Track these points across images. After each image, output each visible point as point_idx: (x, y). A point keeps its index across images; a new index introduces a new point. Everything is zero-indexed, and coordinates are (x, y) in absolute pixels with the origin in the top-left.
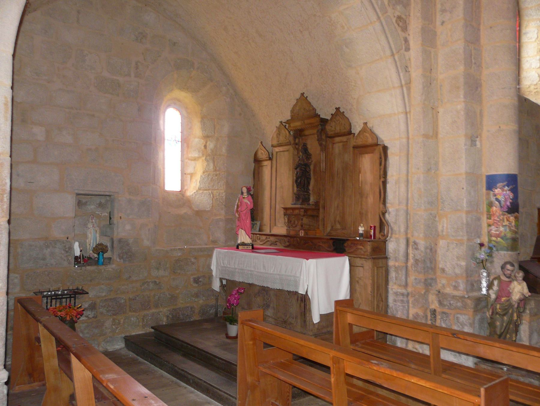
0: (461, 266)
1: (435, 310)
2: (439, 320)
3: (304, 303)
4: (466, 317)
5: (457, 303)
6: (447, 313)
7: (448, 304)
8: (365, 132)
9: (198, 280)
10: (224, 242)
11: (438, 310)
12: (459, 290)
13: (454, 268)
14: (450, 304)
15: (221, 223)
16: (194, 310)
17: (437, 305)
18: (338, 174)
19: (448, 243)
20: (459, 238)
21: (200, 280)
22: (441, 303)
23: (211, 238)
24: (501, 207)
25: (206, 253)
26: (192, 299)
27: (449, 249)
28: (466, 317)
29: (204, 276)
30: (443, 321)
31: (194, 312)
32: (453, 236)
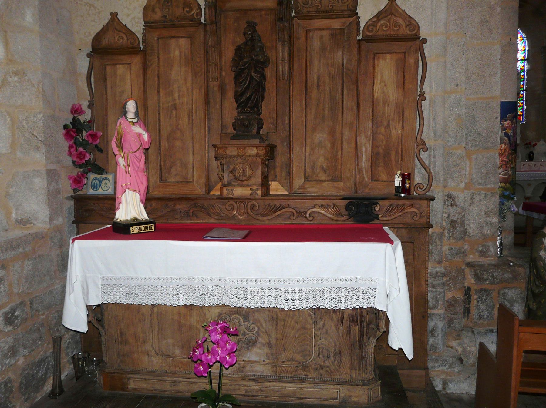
0: (491, 224)
1: (469, 289)
2: (475, 301)
3: (361, 325)
4: (518, 291)
5: (503, 274)
6: (488, 290)
7: (490, 278)
8: (392, 14)
9: (13, 314)
10: (48, 220)
11: (474, 287)
12: (489, 256)
13: (482, 227)
14: (493, 277)
15: (37, 181)
16: (10, 387)
17: (473, 281)
18: (318, 86)
19: (473, 194)
20: (489, 186)
21: (16, 314)
22: (478, 278)
23: (14, 215)
24: (510, 144)
25: (21, 250)
26: (5, 364)
27: (473, 202)
28: (518, 291)
29: (22, 304)
30: (481, 301)
31: (11, 392)
32: (480, 184)
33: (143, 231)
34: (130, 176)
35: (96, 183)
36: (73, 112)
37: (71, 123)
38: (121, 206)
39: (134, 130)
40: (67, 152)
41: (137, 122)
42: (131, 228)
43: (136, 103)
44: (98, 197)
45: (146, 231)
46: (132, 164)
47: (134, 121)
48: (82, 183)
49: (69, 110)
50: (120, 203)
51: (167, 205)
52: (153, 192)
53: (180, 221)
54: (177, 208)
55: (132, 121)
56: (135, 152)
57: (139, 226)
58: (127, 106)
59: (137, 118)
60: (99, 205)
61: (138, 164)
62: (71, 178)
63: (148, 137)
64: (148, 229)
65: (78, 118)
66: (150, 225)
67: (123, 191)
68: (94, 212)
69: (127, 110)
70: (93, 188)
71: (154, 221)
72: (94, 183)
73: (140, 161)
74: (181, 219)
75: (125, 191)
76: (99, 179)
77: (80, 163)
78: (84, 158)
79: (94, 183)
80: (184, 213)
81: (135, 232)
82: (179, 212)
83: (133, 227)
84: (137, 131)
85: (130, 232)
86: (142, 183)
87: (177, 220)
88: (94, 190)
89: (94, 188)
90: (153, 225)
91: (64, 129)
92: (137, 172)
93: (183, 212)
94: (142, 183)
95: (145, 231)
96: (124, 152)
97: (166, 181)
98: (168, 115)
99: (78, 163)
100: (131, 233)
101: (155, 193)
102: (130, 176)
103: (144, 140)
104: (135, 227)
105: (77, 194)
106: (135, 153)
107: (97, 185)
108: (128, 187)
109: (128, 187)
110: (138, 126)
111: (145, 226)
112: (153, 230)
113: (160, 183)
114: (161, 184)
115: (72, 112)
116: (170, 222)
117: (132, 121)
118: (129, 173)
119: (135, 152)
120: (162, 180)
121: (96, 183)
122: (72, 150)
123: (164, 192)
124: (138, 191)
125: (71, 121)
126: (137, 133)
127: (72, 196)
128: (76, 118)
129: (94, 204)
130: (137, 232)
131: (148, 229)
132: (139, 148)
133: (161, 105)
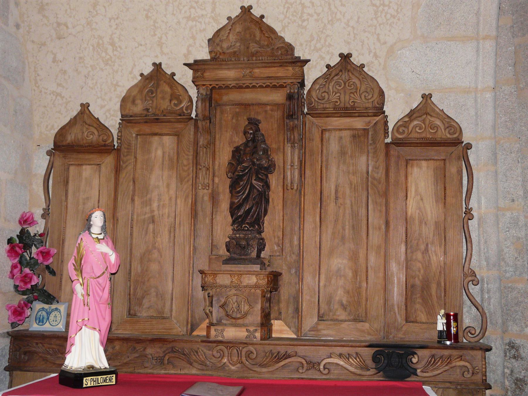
33: (101, 384)
35: (43, 316)
36: (22, 222)
37: (17, 236)
38: (73, 348)
39: (99, 249)
40: (9, 273)
41: (103, 239)
42: (85, 379)
43: (104, 215)
44: (43, 335)
46: (93, 293)
47: (99, 238)
48: (23, 315)
50: (72, 345)
52: (117, 329)
53: (150, 371)
54: (147, 353)
55: (97, 238)
56: (99, 277)
57: (95, 377)
58: (92, 219)
59: (104, 234)
60: (44, 346)
61: (101, 293)
62: (10, 308)
64: (108, 381)
65: (27, 230)
66: (110, 376)
67: (78, 329)
68: (36, 354)
70: (37, 322)
72: (40, 315)
73: (104, 289)
75: (81, 329)
76: (47, 310)
78: (30, 282)
79: (40, 315)
81: (89, 385)
84: (102, 251)
86: (104, 319)
90: (114, 375)
91: (8, 244)
92: (98, 304)
93: (156, 358)
94: (104, 319)
98: (143, 229)
100: (84, 386)
101: (119, 332)
104: (90, 378)
105: (15, 329)
107: (43, 318)
108: (85, 323)
110: (104, 244)
111: (103, 376)
112: (114, 383)
114: (129, 319)
116: (137, 371)
117: (97, 238)
118: (87, 305)
119: (99, 277)
120: (129, 314)
121: (43, 316)
122: (16, 271)
124: (98, 329)
126: (102, 253)
129: (37, 344)
130: (92, 385)
132: (104, 272)
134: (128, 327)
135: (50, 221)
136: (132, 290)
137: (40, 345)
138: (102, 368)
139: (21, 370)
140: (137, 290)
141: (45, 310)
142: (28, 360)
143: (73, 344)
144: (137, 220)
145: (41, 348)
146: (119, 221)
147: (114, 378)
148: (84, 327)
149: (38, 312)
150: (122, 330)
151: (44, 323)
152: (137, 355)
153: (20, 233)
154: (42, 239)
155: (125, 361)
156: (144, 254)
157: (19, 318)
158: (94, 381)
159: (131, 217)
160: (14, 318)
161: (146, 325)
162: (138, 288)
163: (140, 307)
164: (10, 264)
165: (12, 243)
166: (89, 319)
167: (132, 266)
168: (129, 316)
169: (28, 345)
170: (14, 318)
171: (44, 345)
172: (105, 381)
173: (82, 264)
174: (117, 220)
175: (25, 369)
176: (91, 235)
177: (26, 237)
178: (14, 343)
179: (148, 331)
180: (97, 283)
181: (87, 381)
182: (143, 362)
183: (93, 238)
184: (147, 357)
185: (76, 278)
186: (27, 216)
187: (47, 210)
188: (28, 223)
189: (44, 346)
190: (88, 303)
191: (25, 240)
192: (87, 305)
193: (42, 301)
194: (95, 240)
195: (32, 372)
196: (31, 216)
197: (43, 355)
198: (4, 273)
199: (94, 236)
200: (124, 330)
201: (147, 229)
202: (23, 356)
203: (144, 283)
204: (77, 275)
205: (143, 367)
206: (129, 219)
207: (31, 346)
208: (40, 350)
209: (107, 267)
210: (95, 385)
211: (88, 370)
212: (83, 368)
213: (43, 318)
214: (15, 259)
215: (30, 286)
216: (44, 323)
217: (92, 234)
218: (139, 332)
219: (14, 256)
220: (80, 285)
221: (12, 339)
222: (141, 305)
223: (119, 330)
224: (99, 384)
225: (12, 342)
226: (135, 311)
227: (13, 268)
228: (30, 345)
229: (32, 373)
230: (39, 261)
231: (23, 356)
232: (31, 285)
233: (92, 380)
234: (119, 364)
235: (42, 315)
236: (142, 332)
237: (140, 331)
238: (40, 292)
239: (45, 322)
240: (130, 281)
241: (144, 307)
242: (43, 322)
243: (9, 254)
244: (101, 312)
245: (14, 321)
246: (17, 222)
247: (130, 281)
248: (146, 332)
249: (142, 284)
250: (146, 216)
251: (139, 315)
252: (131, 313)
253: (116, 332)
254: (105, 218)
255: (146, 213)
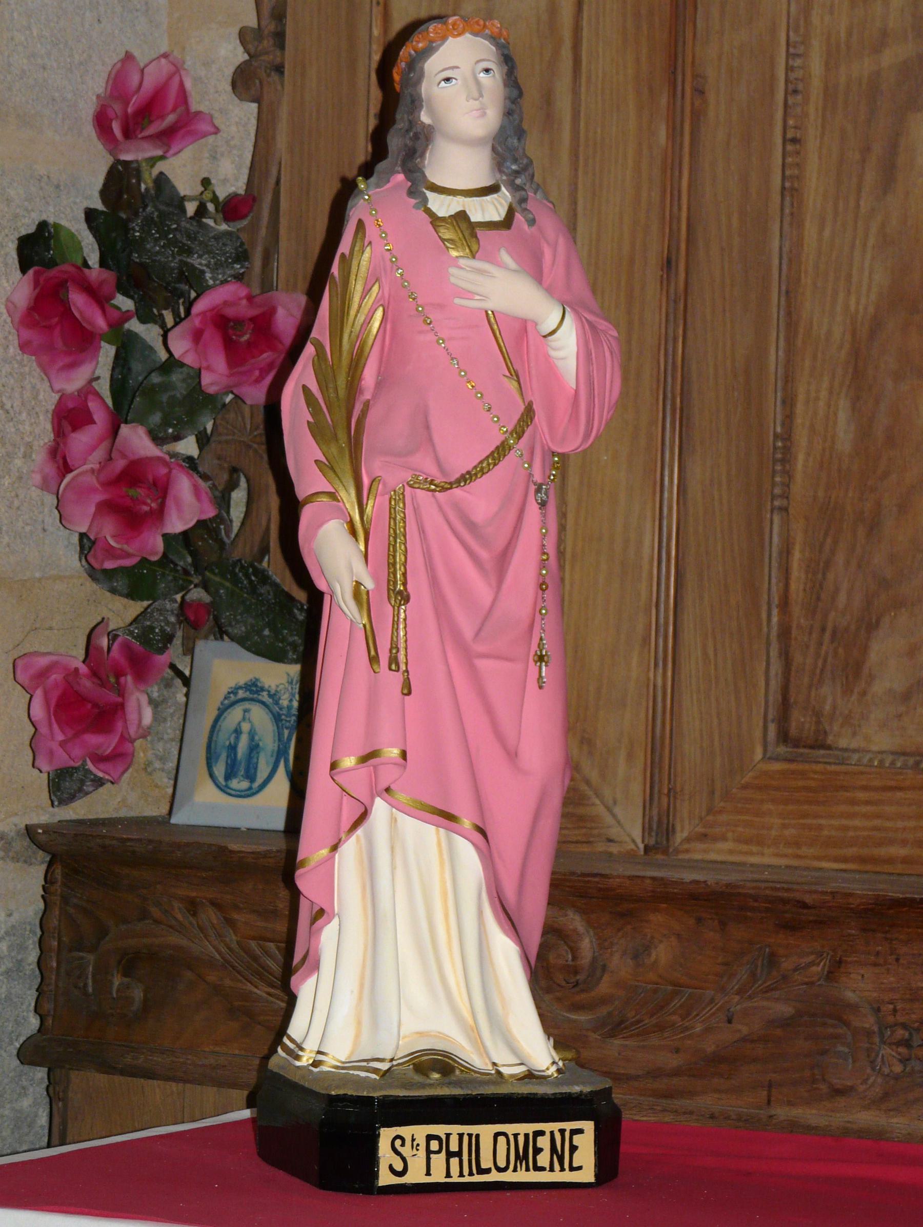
33: (494, 1176)
34: (407, 689)
35: (252, 734)
36: (116, 127)
37: (90, 215)
38: (328, 935)
39: (468, 294)
40: (40, 456)
41: (507, 222)
42: (386, 1135)
43: (508, 60)
44: (223, 850)
45: (558, 1176)
46: (434, 582)
47: (475, 217)
48: (120, 725)
49: (88, 110)
50: (320, 914)
51: (772, 961)
52: (703, 837)
53: (866, 1118)
54: (850, 996)
55: (462, 216)
56: (466, 478)
57: (454, 1129)
58: (425, 89)
59: (515, 188)
60: (230, 923)
61: (483, 590)
62: (42, 675)
63: (586, 356)
64: (544, 1159)
65: (162, 181)
66: (555, 1126)
67: (347, 819)
68: (189, 975)
69: (425, 118)
70: (220, 770)
71: (607, 1092)
72: (238, 732)
73: (503, 558)
74: (885, 1096)
75: (363, 816)
76: (274, 696)
77: (128, 555)
78: (159, 514)
79: (238, 732)
80: (907, 1043)
81: (417, 1175)
82: (869, 1034)
83: (406, 1131)
84: (490, 305)
85: (375, 1175)
86: (512, 755)
87: (841, 1102)
88: (225, 789)
89: (228, 777)
90: (588, 1126)
91: (24, 269)
92: (468, 657)
93: (901, 1033)
94: (512, 755)
95: (509, 1177)
96: (366, 481)
97: (820, 743)
98: (866, 150)
99: (111, 553)
100: (385, 1178)
101: (719, 852)
102: (407, 689)
103: (550, 370)
104: (420, 1131)
105: (78, 810)
106: (457, 492)
107: (254, 748)
108: (387, 776)
109: (387, 776)
110: (505, 257)
111: (510, 1129)
112: (587, 1175)
113: (766, 758)
114: (778, 766)
115: (102, 122)
116: (782, 1113)
117: (462, 216)
118: (393, 660)
119: (466, 478)
120: (784, 737)
121: (252, 734)
122: (81, 440)
123: (797, 845)
124: (467, 824)
125: (99, 205)
126: (491, 319)
127: (30, 831)
128: (138, 173)
129: (193, 906)
130: (438, 1176)
131: (544, 1159)
132: (502, 450)
133: (816, 66)
134: (778, 821)
135: (284, 112)
136: (797, 572)
137: (210, 915)
138: (506, 1071)
139: (108, 1068)
140: (831, 576)
141: (264, 696)
142: (146, 1007)
143: (321, 912)
144: (829, 93)
145: (220, 936)
146: (711, 97)
147: (586, 1143)
148: (380, 807)
149: (222, 711)
150: (738, 840)
151: (259, 781)
152: (785, 1009)
153: (105, 193)
154: (244, 237)
155: (709, 1046)
156: (876, 325)
157: (93, 739)
158: (450, 1155)
159: (789, 69)
160: (62, 744)
161: (889, 809)
162: (840, 558)
163: (848, 690)
164: (49, 400)
165: (51, 264)
166: (404, 755)
167: (800, 408)
168: (782, 749)
169: (144, 915)
170: (62, 744)
171: (236, 916)
172: (522, 1158)
173: (367, 396)
174: (700, 92)
175: (128, 1059)
176: (425, 200)
177: (149, 222)
178: (65, 900)
179: (903, 852)
180: (452, 516)
181: (406, 1151)
182: (824, 1052)
183: (435, 220)
184: (847, 1024)
185: (322, 484)
186: (149, 84)
187: (267, 43)
188: (152, 130)
189: (230, 923)
190: (394, 646)
191: (139, 245)
192: (393, 660)
193: (241, 641)
194: (447, 234)
195: (173, 1079)
196: (175, 81)
197: (228, 982)
198: (10, 456)
199: (443, 206)
200: (748, 841)
201: (893, 147)
202: (117, 981)
203: (873, 527)
204: (328, 468)
205: (824, 1087)
206: (773, 77)
207: (157, 922)
208: (207, 948)
209: (529, 412)
210: (455, 1179)
211: (418, 1078)
212: (384, 1066)
213: (254, 748)
214: (72, 366)
215: (160, 545)
216: (259, 781)
217: (430, 195)
218: (845, 860)
219: (59, 344)
220: (348, 538)
221: (58, 872)
222: (857, 673)
223: (715, 839)
224: (482, 1171)
225: (57, 888)
226: (818, 714)
227: (67, 427)
228: (155, 911)
229: (174, 1087)
230: (206, 379)
231: (117, 981)
232: (165, 536)
233: (434, 1145)
234: (674, 1061)
235: (245, 727)
236: (862, 860)
237: (851, 851)
238: (235, 581)
239: (263, 772)
240: (784, 510)
241: (878, 688)
242: (250, 776)
243: (27, 334)
244: (489, 710)
245: (63, 759)
246: (89, 129)
247: (784, 510)
248: (890, 861)
249: (861, 532)
250: (889, 57)
251: (843, 743)
252: (793, 731)
253: (699, 852)
254: (512, 80)
255: (884, 33)
